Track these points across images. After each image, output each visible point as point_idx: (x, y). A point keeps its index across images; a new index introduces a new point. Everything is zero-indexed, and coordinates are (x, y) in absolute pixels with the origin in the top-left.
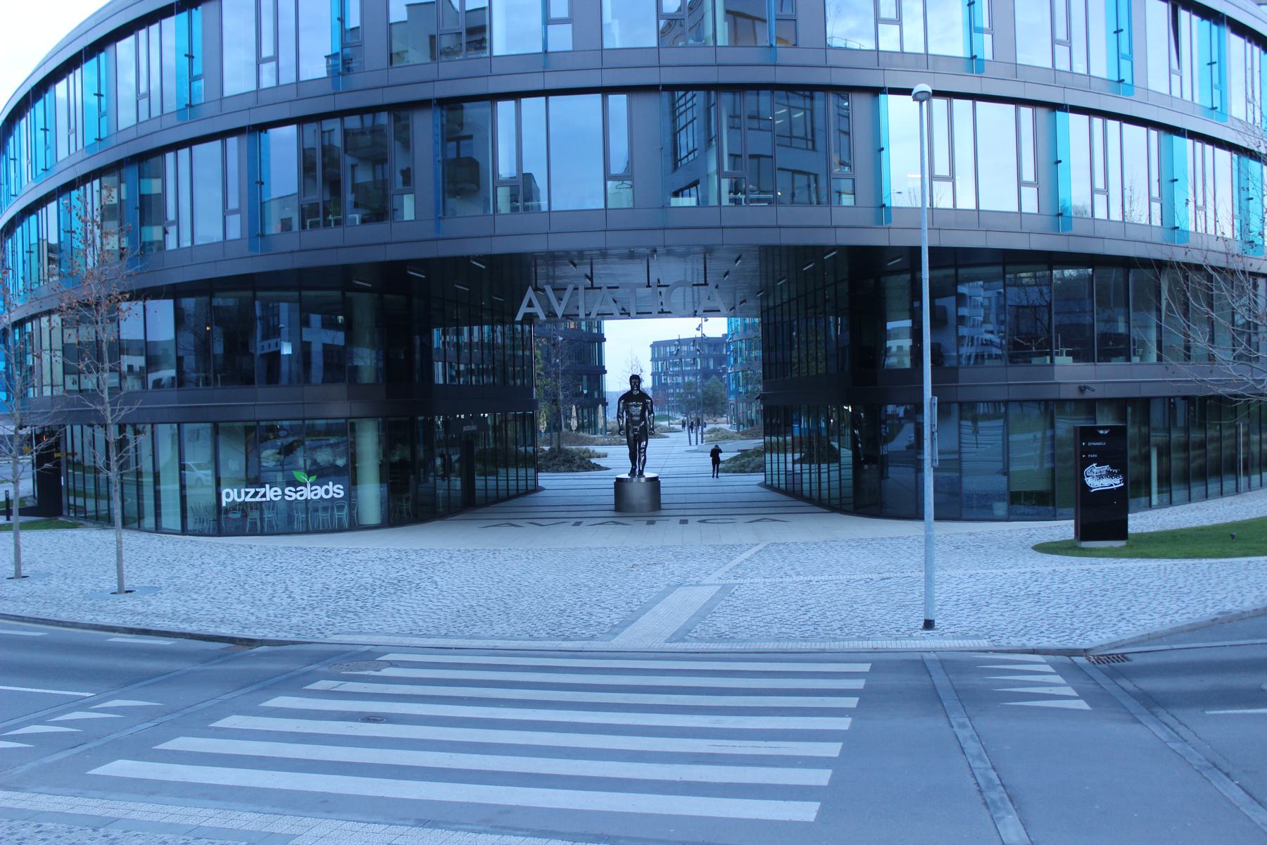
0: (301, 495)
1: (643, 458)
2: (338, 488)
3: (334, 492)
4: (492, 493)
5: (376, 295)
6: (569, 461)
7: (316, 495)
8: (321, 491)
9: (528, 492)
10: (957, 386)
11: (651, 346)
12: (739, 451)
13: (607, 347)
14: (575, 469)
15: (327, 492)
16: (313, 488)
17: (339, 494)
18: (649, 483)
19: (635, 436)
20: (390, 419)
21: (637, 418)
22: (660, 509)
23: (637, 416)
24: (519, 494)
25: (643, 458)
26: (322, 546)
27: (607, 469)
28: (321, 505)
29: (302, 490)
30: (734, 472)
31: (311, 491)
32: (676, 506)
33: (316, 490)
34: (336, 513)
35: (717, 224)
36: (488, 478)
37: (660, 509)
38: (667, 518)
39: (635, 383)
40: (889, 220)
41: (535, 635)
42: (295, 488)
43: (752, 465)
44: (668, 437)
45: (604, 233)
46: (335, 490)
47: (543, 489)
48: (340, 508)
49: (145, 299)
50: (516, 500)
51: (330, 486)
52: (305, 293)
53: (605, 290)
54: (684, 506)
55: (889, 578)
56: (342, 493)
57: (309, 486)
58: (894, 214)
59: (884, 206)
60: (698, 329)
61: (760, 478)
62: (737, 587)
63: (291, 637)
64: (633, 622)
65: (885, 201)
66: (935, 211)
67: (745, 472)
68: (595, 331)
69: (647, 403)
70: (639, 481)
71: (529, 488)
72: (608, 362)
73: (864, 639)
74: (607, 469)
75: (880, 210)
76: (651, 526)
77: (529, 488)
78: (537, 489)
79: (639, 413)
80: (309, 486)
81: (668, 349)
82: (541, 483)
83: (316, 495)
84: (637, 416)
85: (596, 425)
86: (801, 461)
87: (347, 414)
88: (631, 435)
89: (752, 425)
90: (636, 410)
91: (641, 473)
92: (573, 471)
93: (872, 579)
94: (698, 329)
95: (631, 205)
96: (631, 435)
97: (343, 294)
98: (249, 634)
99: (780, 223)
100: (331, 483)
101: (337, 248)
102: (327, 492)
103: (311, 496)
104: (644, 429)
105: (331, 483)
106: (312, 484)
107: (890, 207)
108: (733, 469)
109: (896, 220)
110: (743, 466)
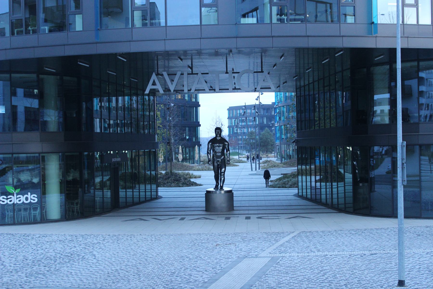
0: (11, 201)
1: (223, 179)
2: (34, 197)
3: (31, 199)
6: (177, 180)
7: (20, 201)
10: (418, 135)
11: (228, 109)
12: (282, 174)
14: (181, 185)
15: (27, 199)
16: (18, 196)
17: (34, 200)
18: (226, 194)
19: (218, 165)
20: (66, 154)
21: (219, 154)
22: (233, 210)
23: (219, 152)
25: (223, 179)
30: (279, 187)
31: (17, 198)
32: (243, 208)
33: (20, 197)
34: (32, 212)
37: (233, 210)
39: (218, 132)
40: (376, 32)
42: (7, 196)
43: (290, 183)
44: (238, 166)
48: (35, 209)
51: (29, 195)
52: (13, 75)
56: (36, 200)
57: (15, 195)
58: (379, 28)
59: (373, 23)
60: (257, 99)
64: (217, 280)
65: (374, 20)
67: (286, 188)
68: (194, 100)
69: (226, 145)
70: (220, 193)
71: (153, 196)
72: (201, 120)
79: (220, 151)
80: (15, 195)
82: (160, 194)
83: (20, 201)
84: (219, 152)
85: (194, 158)
87: (40, 150)
88: (216, 164)
90: (219, 149)
92: (180, 186)
93: (365, 255)
94: (257, 99)
96: (216, 164)
97: (38, 76)
100: (29, 193)
101: (34, 47)
103: (17, 201)
105: (29, 193)
106: (18, 194)
107: (377, 24)
108: (279, 186)
110: (284, 183)
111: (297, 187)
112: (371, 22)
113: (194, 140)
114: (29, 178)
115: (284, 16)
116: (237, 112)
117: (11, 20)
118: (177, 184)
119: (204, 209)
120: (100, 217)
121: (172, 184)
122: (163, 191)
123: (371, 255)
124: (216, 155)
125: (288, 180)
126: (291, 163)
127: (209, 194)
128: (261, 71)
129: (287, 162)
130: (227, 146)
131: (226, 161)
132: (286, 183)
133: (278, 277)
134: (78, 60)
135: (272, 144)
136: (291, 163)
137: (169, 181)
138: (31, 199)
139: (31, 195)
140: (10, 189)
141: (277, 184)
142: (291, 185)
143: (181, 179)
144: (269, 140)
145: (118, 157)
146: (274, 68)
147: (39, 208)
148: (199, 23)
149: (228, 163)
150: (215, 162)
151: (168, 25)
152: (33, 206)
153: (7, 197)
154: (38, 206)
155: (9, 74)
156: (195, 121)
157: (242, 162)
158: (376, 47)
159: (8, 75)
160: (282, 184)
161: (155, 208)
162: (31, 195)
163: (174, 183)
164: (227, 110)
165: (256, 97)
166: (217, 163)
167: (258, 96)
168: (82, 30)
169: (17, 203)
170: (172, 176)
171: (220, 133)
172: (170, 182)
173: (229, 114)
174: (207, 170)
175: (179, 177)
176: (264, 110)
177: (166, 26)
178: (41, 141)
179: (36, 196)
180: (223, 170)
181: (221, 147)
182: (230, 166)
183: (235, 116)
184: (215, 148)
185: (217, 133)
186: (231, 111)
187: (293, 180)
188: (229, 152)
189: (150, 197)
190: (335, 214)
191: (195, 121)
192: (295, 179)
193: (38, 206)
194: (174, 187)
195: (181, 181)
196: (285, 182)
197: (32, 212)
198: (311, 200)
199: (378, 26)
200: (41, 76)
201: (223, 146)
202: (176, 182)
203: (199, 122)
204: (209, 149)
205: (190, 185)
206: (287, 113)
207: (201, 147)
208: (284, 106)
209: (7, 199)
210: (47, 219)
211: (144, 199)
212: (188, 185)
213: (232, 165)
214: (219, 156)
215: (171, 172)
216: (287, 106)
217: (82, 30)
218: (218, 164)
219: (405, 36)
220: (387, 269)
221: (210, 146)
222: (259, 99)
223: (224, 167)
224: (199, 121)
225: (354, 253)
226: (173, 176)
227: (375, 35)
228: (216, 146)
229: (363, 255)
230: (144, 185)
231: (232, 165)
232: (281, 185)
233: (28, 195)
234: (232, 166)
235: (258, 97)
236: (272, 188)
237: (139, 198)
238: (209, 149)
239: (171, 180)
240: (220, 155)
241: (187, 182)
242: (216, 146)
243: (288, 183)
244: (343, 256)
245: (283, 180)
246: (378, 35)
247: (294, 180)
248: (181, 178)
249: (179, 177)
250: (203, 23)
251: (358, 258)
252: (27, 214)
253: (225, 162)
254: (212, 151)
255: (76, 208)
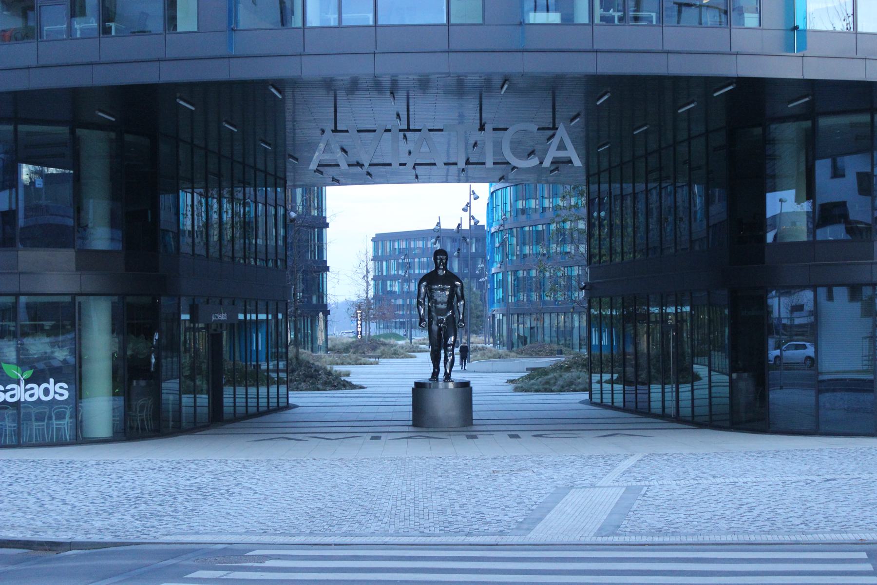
0: (12, 396)
1: (450, 358)
2: (61, 388)
3: (55, 393)
4: (241, 410)
5: (113, 135)
6: (311, 377)
7: (32, 395)
8: (38, 391)
9: (279, 409)
10: (872, 264)
11: (373, 240)
12: (528, 369)
13: (330, 234)
14: (320, 386)
15: (46, 392)
16: (29, 386)
17: (61, 395)
18: (460, 389)
19: (440, 329)
20: (129, 299)
21: (444, 306)
22: (472, 424)
23: (442, 303)
24: (269, 411)
25: (450, 358)
26: (57, 458)
27: (361, 387)
28: (34, 411)
29: (13, 389)
30: (537, 391)
31: (26, 390)
32: (489, 422)
33: (32, 389)
34: (54, 422)
35: (589, 47)
36: (197, 396)
37: (472, 424)
38: (492, 433)
39: (441, 260)
40: (803, 46)
41: (426, 531)
43: (560, 382)
44: (415, 357)
45: (447, 54)
46: (59, 391)
47: (295, 406)
48: (60, 416)
49: (340, 27)
50: (273, 415)
51: (51, 385)
52: (22, 128)
53: (425, 131)
54: (500, 422)
55: (835, 479)
56: (66, 394)
58: (810, 40)
59: (796, 28)
60: (465, 210)
61: (585, 396)
62: (645, 488)
63: (108, 538)
64: (540, 519)
65: (799, 22)
66: (859, 36)
67: (552, 391)
68: (315, 213)
69: (456, 286)
70: (446, 387)
71: (281, 405)
72: (332, 256)
73: (840, 532)
74: (361, 387)
75: (792, 33)
76: (471, 440)
77: (261, 409)
78: (288, 407)
79: (446, 300)
80: (23, 383)
81: (396, 245)
82: (291, 401)
83: (32, 395)
84: (442, 303)
85: (314, 339)
86: (612, 382)
87: (75, 289)
88: (435, 328)
89: (525, 343)
90: (442, 295)
91: (448, 377)
92: (318, 389)
93: (813, 481)
94: (465, 210)
95: (480, 21)
96: (435, 328)
97: (72, 132)
98: (50, 536)
99: (666, 48)
100: (52, 381)
101: (92, 64)
102: (46, 392)
103: (25, 397)
104: (452, 321)
105: (52, 381)
106: (27, 382)
107: (805, 31)
108: (536, 387)
109: (813, 47)
110: (547, 383)
111: (584, 390)
112: (792, 26)
113: (314, 300)
114: (48, 350)
115: (614, 11)
116: (393, 245)
117: (40, 6)
118: (312, 384)
119: (411, 423)
120: (193, 436)
121: (300, 384)
122: (295, 397)
123: (825, 481)
124: (435, 307)
125: (555, 376)
126: (533, 351)
127: (423, 389)
128: (551, 126)
129: (524, 350)
130: (460, 290)
131: (457, 322)
132: (552, 382)
133: (661, 514)
134: (178, 95)
135: (479, 314)
136: (533, 351)
137: (293, 378)
138: (55, 393)
139: (55, 383)
140: (13, 371)
141: (533, 384)
142: (563, 387)
143: (319, 375)
144: (473, 305)
145: (222, 311)
146: (573, 123)
147: (68, 415)
148: (445, 21)
149: (461, 325)
150: (433, 323)
151: (380, 23)
152: (55, 409)
153: (5, 388)
154: (66, 408)
155: (11, 124)
156: (317, 259)
157: (419, 350)
158: (801, 77)
159: (11, 128)
160: (543, 385)
161: (286, 427)
162: (55, 383)
163: (305, 381)
164: (372, 240)
165: (464, 206)
166: (438, 325)
167: (468, 203)
168: (196, 30)
169: (26, 401)
170: (301, 366)
171: (444, 261)
172: (296, 381)
173: (376, 249)
174: (353, 363)
175: (316, 370)
176: (453, 242)
177: (376, 25)
178: (77, 269)
179: (65, 386)
180: (451, 340)
181: (447, 290)
182: (397, 358)
183: (388, 254)
184: (433, 292)
185: (438, 261)
186: (380, 244)
187: (566, 377)
188: (462, 302)
189: (276, 405)
190: (692, 430)
191: (317, 259)
192: (570, 374)
193: (66, 408)
194: (306, 390)
195: (321, 378)
196: (550, 379)
197: (54, 422)
198: (624, 409)
199: (808, 34)
200: (80, 132)
201: (450, 288)
202: (308, 379)
203: (326, 262)
204: (422, 296)
205: (340, 386)
206: (518, 247)
207: (328, 316)
208: (511, 229)
209: (5, 392)
210: (84, 438)
211: (256, 408)
212: (335, 386)
213: (403, 356)
214: (441, 310)
215: (297, 358)
216: (518, 229)
217: (196, 30)
218: (440, 326)
219: (859, 55)
220: (872, 501)
221: (423, 290)
222: (469, 208)
223: (453, 334)
224: (325, 259)
225: (789, 478)
226: (303, 368)
227: (800, 54)
228: (436, 289)
229: (809, 481)
230: (232, 388)
231: (403, 356)
232: (541, 387)
233: (49, 383)
234: (402, 358)
235: (467, 205)
236: (521, 392)
237: (247, 407)
238: (422, 296)
239: (299, 375)
240: (445, 309)
241: (333, 380)
242: (436, 289)
243: (555, 383)
244: (771, 483)
245: (538, 379)
246: (806, 53)
247: (568, 377)
248: (320, 372)
249: (316, 370)
250: (452, 21)
251: (802, 486)
252: (43, 425)
253: (455, 322)
254: (426, 300)
255: (140, 416)
